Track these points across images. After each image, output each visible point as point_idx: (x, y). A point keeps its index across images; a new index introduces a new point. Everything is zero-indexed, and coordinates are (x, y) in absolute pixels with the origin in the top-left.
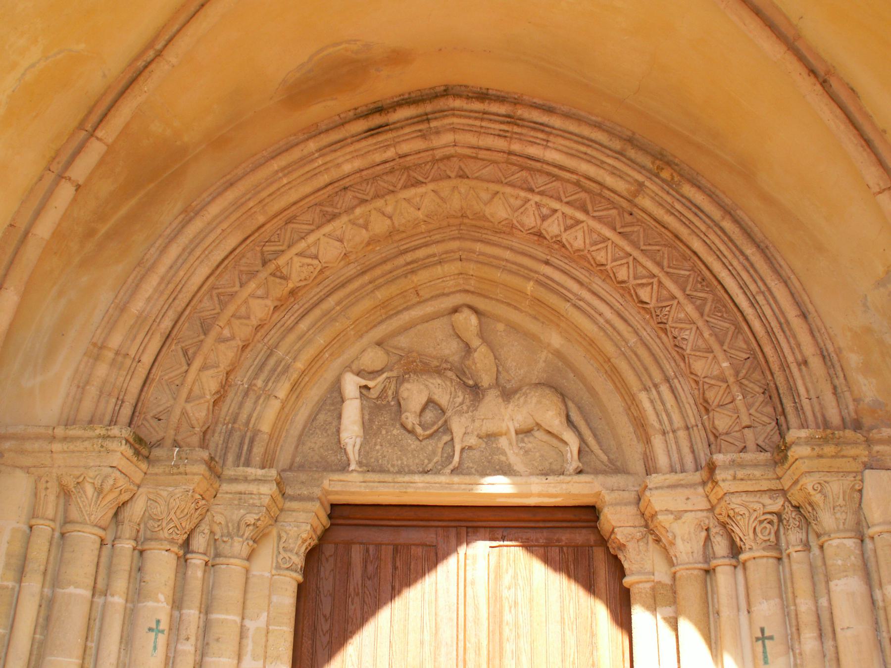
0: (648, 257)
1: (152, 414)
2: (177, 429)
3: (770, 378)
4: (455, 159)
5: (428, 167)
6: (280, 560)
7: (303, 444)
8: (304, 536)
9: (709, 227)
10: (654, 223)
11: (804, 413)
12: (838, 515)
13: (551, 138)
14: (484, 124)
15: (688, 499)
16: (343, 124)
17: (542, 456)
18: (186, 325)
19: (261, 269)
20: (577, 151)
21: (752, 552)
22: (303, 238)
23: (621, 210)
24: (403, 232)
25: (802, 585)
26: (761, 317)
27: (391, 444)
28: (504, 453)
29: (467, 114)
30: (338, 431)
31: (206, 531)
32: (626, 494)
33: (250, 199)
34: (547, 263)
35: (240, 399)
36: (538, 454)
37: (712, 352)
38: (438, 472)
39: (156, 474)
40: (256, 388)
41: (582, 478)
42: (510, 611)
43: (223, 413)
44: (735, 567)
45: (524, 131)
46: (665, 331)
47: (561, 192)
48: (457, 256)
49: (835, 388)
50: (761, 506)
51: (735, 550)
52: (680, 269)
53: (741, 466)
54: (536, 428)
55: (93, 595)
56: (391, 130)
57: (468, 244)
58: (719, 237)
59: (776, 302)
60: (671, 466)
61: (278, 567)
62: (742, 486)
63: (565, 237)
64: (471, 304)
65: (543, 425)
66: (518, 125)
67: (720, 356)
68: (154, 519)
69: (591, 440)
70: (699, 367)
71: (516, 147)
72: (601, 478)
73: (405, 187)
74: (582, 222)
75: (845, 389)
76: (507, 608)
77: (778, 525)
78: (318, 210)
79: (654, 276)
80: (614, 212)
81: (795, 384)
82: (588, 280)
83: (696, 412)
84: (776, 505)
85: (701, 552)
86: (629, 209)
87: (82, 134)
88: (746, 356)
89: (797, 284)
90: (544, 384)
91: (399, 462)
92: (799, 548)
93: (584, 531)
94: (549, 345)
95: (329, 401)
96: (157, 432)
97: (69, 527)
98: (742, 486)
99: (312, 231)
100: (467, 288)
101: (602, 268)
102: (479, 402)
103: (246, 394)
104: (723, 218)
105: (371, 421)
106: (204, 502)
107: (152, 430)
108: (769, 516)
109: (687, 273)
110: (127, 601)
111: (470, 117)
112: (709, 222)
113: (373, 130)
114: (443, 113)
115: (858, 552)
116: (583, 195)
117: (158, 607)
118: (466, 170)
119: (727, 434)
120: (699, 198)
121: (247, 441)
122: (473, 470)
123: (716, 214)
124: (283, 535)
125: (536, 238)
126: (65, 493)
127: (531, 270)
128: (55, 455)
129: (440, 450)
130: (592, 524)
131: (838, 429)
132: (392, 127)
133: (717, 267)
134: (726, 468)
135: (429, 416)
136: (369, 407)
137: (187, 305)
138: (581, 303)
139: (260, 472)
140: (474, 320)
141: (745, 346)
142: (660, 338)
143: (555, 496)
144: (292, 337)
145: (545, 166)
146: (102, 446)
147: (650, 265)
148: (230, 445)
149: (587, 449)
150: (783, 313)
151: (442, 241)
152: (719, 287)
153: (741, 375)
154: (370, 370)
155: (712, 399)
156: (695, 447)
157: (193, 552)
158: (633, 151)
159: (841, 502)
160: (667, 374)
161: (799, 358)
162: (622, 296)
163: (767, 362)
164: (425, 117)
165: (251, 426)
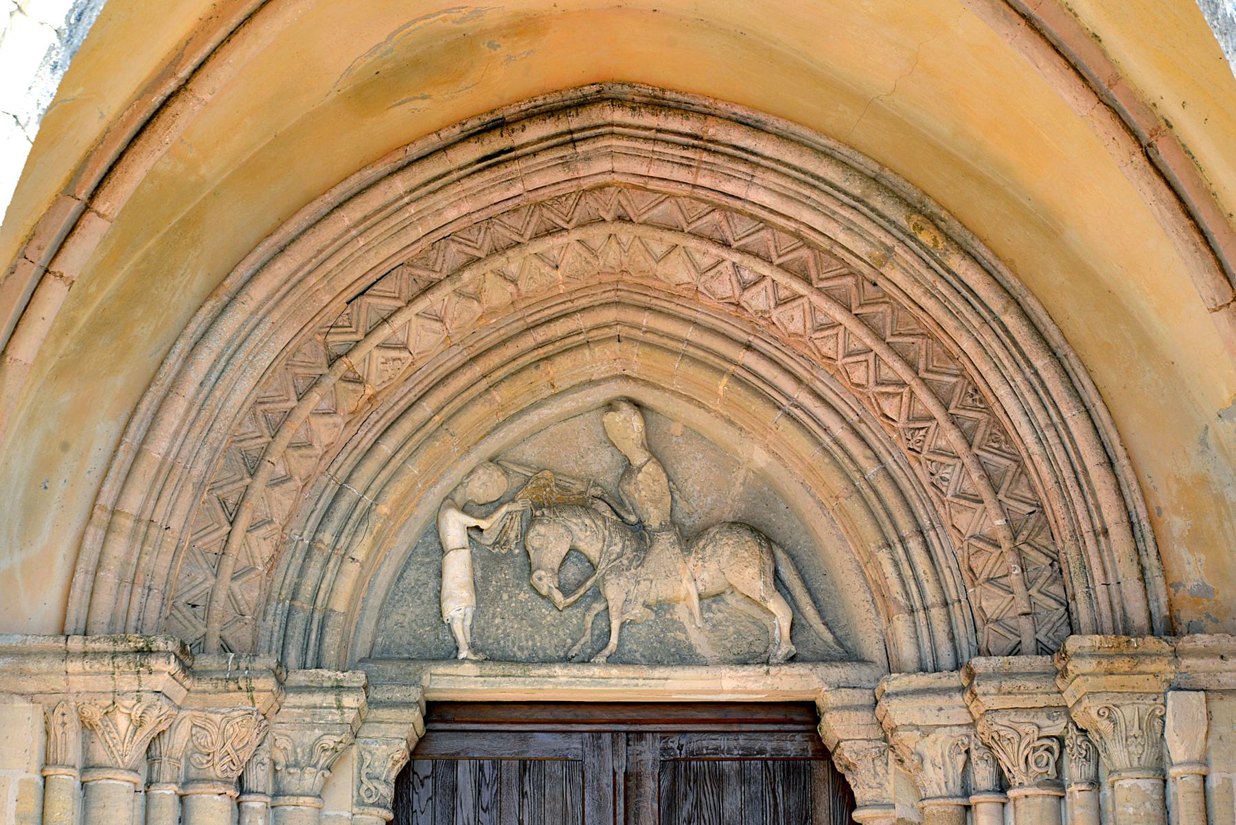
5: (571, 202)
6: (371, 801)
7: (387, 617)
8: (397, 756)
12: (1132, 749)
13: (758, 173)
15: (940, 709)
17: (738, 633)
19: (327, 371)
27: (517, 616)
29: (632, 131)
31: (266, 760)
33: (310, 272)
34: (749, 347)
35: (300, 561)
36: (731, 629)
37: (982, 502)
38: (586, 661)
39: (205, 692)
40: (323, 547)
41: (798, 669)
45: (719, 160)
47: (772, 249)
49: (1143, 571)
50: (1035, 728)
53: (1010, 675)
54: (728, 592)
60: (920, 659)
61: (361, 803)
62: (1011, 702)
63: (775, 315)
64: (633, 396)
65: (740, 588)
68: (201, 753)
72: (821, 668)
73: (537, 236)
74: (801, 296)
78: (405, 276)
87: (75, 207)
88: (1030, 509)
89: (1104, 415)
91: (530, 643)
93: (798, 737)
95: (421, 550)
97: (94, 775)
98: (1011, 702)
99: (399, 309)
102: (646, 552)
105: (485, 579)
107: (186, 623)
108: (1047, 742)
109: (954, 380)
114: (598, 132)
116: (805, 253)
118: (629, 209)
120: (974, 277)
121: (315, 626)
122: (638, 655)
123: (996, 302)
124: (368, 757)
126: (87, 728)
128: (71, 678)
132: (519, 152)
134: (988, 677)
136: (481, 558)
138: (797, 412)
140: (637, 422)
143: (757, 693)
144: (371, 466)
150: (1080, 457)
151: (590, 308)
155: (980, 569)
156: (956, 632)
157: (250, 792)
164: (568, 137)
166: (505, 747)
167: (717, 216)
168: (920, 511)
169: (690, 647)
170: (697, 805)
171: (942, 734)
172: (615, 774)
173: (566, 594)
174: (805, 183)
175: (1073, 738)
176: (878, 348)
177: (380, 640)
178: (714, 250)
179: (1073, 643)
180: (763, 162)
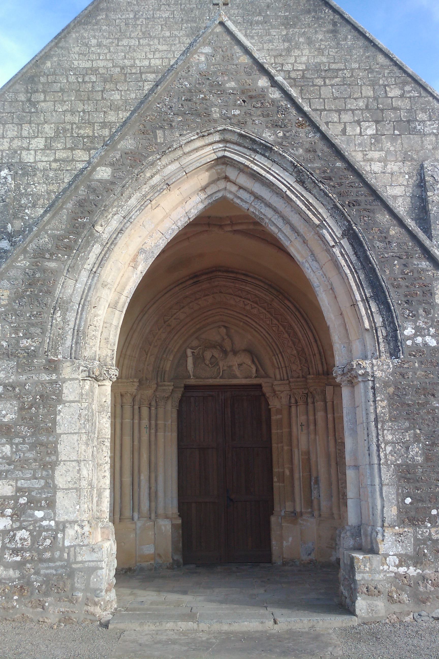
21: (300, 402)
34: (246, 316)
41: (257, 379)
53: (297, 382)
69: (259, 367)
84: (306, 392)
116: (257, 299)
117: (145, 422)
140: (225, 330)
167: (240, 292)
168: (281, 349)
171: (285, 392)
175: (309, 394)
176: (272, 318)
178: (239, 298)
179: (308, 377)
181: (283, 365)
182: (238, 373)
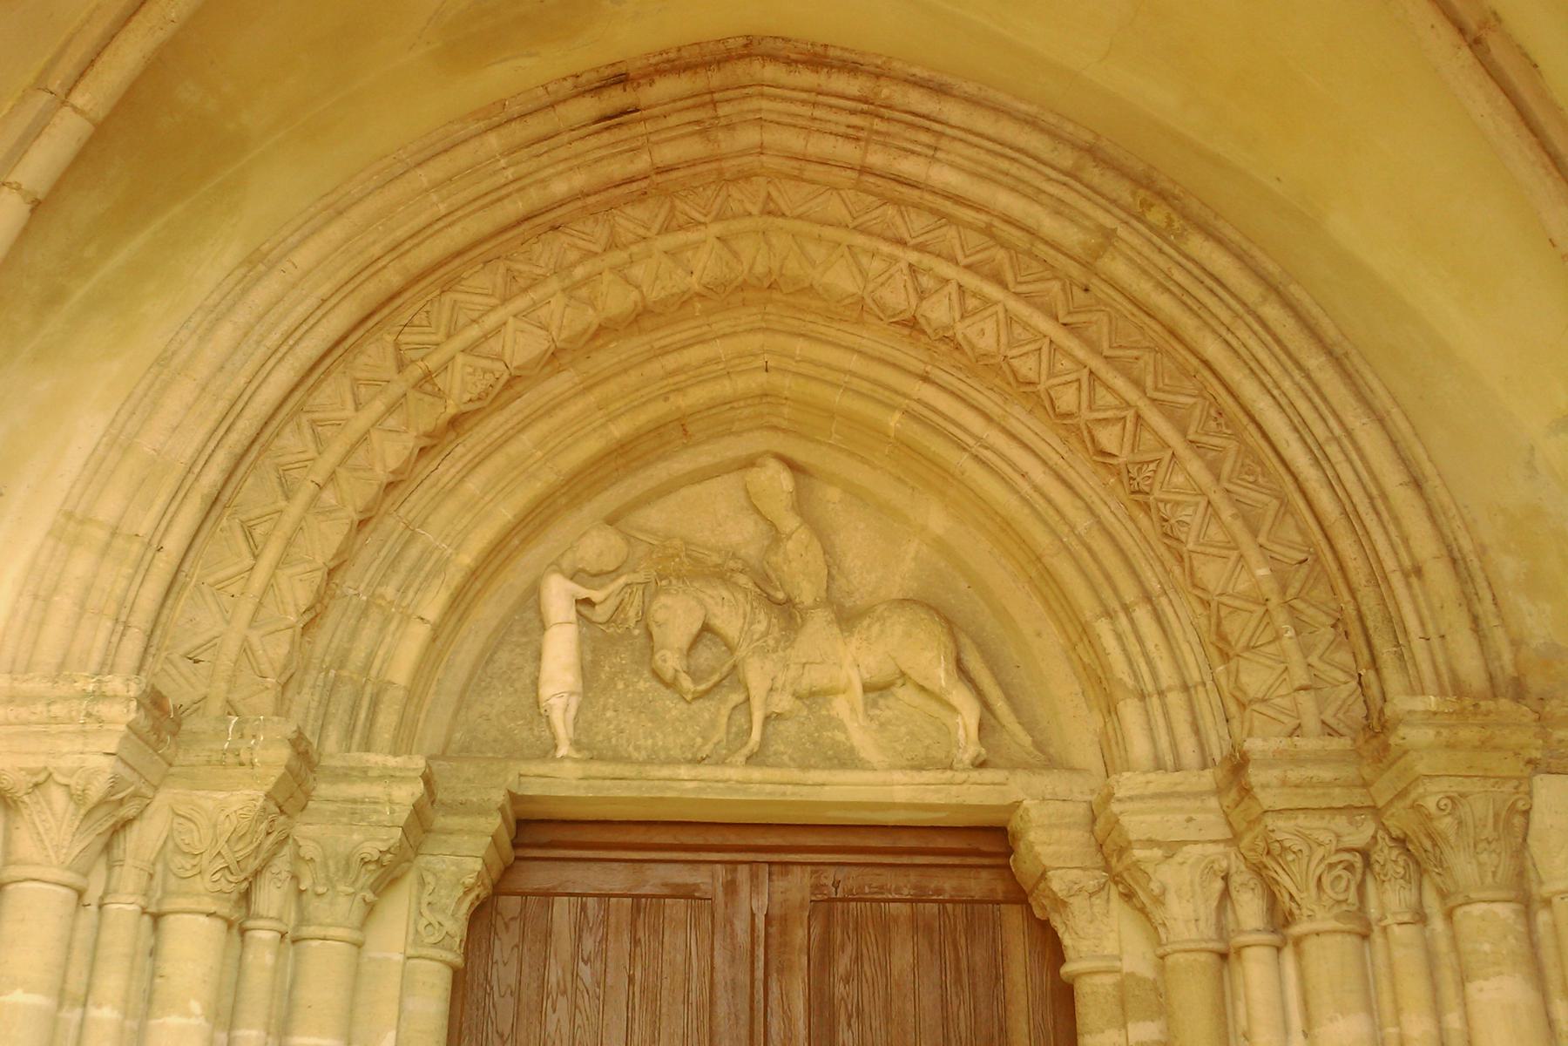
0: (1116, 369)
1: (182, 651)
2: (232, 680)
3: (1347, 597)
4: (762, 180)
5: (709, 192)
6: (421, 928)
8: (469, 880)
9: (1237, 316)
10: (1130, 307)
11: (1415, 665)
13: (944, 143)
14: (818, 113)
15: (1190, 820)
16: (552, 106)
17: (911, 733)
18: (250, 481)
20: (992, 168)
21: (1317, 917)
22: (474, 321)
23: (1068, 283)
24: (660, 314)
25: (1414, 987)
26: (1333, 483)
27: (633, 708)
28: (842, 727)
30: (535, 683)
31: (284, 875)
32: (1069, 808)
34: (925, 379)
35: (353, 621)
36: (903, 730)
38: (722, 762)
41: (988, 775)
42: (849, 1025)
43: (318, 651)
44: (1279, 949)
45: (895, 128)
46: (1146, 508)
47: (958, 246)
48: (760, 363)
49: (1475, 619)
50: (1332, 837)
51: (1279, 918)
52: (1175, 393)
54: (899, 682)
55: (60, 1005)
56: (645, 120)
57: (781, 341)
58: (1255, 333)
59: (1362, 457)
63: (960, 329)
64: (781, 450)
65: (914, 676)
66: (882, 118)
67: (1253, 555)
70: (1211, 573)
71: (877, 159)
74: (996, 303)
75: (1495, 622)
76: (843, 1019)
77: (1364, 874)
78: (502, 270)
79: (1129, 405)
80: (1056, 286)
81: (1399, 610)
82: (1001, 412)
83: (1201, 658)
84: (1361, 834)
85: (1213, 920)
86: (1084, 280)
88: (1302, 557)
89: (1403, 425)
90: (915, 602)
91: (650, 742)
92: (1406, 918)
93: (984, 874)
94: (924, 528)
96: (192, 686)
100: (775, 421)
101: (1029, 389)
102: (796, 632)
103: (364, 612)
104: (1265, 299)
106: (282, 818)
108: (1346, 856)
109: (1191, 401)
110: (125, 1015)
111: (792, 101)
112: (1237, 307)
113: (610, 118)
115: (1521, 928)
116: (1000, 255)
119: (1264, 700)
120: (1221, 262)
121: (365, 703)
123: (1251, 290)
124: (429, 878)
125: (906, 331)
127: (896, 392)
129: (725, 720)
130: (999, 861)
131: (1486, 698)
133: (1249, 390)
134: (1268, 764)
135: (705, 656)
137: (253, 442)
139: (392, 761)
140: (786, 480)
141: (1299, 539)
142: (1132, 519)
145: (928, 197)
146: (89, 715)
147: (1120, 383)
148: (332, 709)
149: (993, 721)
150: (1375, 479)
152: (1252, 428)
153: (1292, 591)
154: (594, 571)
156: (1201, 722)
158: (1096, 171)
159: (1488, 832)
160: (1147, 585)
161: (1407, 563)
162: (1065, 441)
163: (1342, 568)
164: (707, 98)
165: (373, 673)
166: (615, 879)
169: (852, 750)
170: (858, 959)
172: (753, 915)
173: (696, 681)
174: (1003, 156)
175: (1385, 854)
177: (458, 735)
180: (948, 131)
181: (1167, 675)
182: (859, 735)
